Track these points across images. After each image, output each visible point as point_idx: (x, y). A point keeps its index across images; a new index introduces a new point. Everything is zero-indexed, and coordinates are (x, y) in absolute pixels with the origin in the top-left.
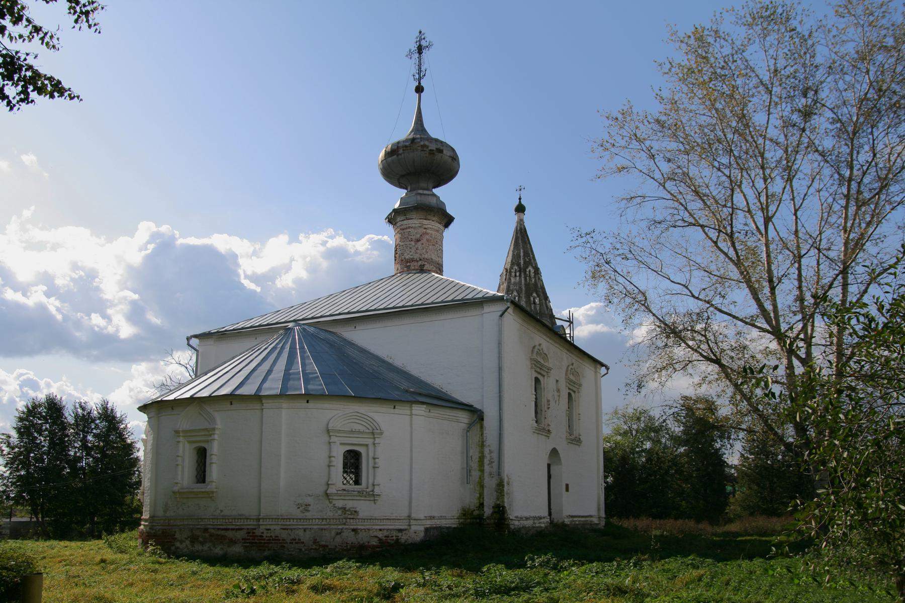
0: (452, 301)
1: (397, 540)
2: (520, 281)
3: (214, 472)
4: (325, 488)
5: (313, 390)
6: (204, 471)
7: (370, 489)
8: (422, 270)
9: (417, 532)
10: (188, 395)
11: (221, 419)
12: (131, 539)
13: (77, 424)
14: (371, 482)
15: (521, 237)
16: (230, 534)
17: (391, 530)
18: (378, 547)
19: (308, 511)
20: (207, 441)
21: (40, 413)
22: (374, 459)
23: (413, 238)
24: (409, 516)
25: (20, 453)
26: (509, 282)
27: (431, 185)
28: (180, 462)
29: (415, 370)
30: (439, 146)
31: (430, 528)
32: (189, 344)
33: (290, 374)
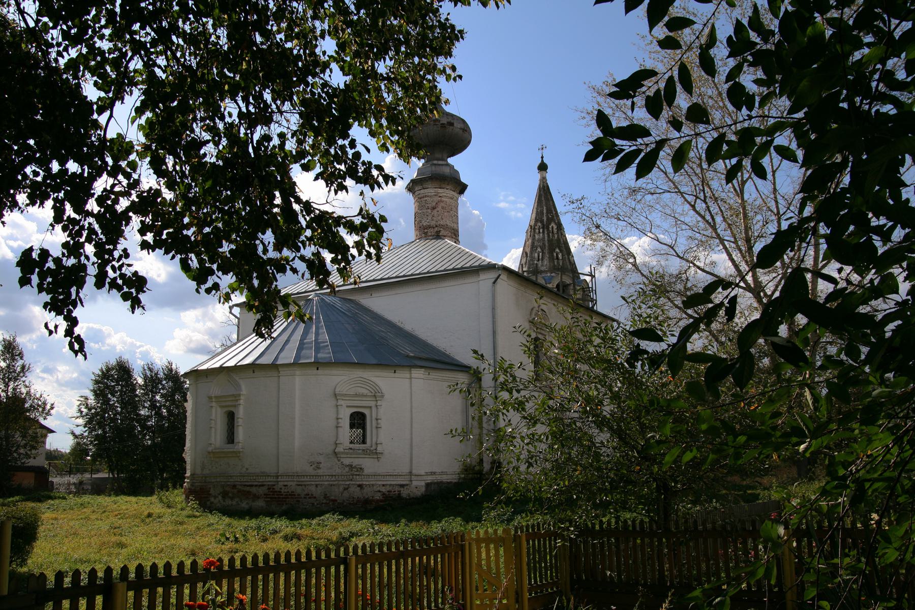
0: (453, 269)
1: (399, 494)
2: (544, 238)
3: (241, 434)
4: (333, 447)
5: (322, 358)
6: (233, 433)
7: (374, 447)
8: (438, 236)
9: (418, 487)
10: (217, 365)
11: (245, 387)
12: (177, 496)
13: (146, 385)
14: (374, 440)
15: (544, 195)
16: (254, 490)
17: (393, 485)
18: (381, 501)
19: (319, 468)
20: (235, 406)
21: (112, 376)
22: (377, 419)
23: (430, 206)
24: (411, 472)
25: (97, 414)
26: (534, 239)
27: (445, 155)
28: (213, 425)
29: (423, 333)
30: (450, 119)
31: (431, 483)
32: (231, 312)
33: (304, 344)
